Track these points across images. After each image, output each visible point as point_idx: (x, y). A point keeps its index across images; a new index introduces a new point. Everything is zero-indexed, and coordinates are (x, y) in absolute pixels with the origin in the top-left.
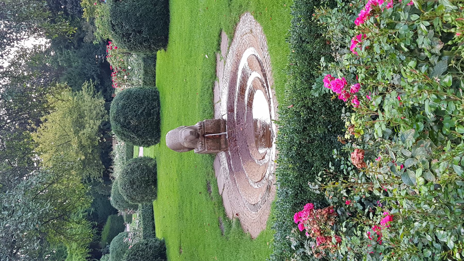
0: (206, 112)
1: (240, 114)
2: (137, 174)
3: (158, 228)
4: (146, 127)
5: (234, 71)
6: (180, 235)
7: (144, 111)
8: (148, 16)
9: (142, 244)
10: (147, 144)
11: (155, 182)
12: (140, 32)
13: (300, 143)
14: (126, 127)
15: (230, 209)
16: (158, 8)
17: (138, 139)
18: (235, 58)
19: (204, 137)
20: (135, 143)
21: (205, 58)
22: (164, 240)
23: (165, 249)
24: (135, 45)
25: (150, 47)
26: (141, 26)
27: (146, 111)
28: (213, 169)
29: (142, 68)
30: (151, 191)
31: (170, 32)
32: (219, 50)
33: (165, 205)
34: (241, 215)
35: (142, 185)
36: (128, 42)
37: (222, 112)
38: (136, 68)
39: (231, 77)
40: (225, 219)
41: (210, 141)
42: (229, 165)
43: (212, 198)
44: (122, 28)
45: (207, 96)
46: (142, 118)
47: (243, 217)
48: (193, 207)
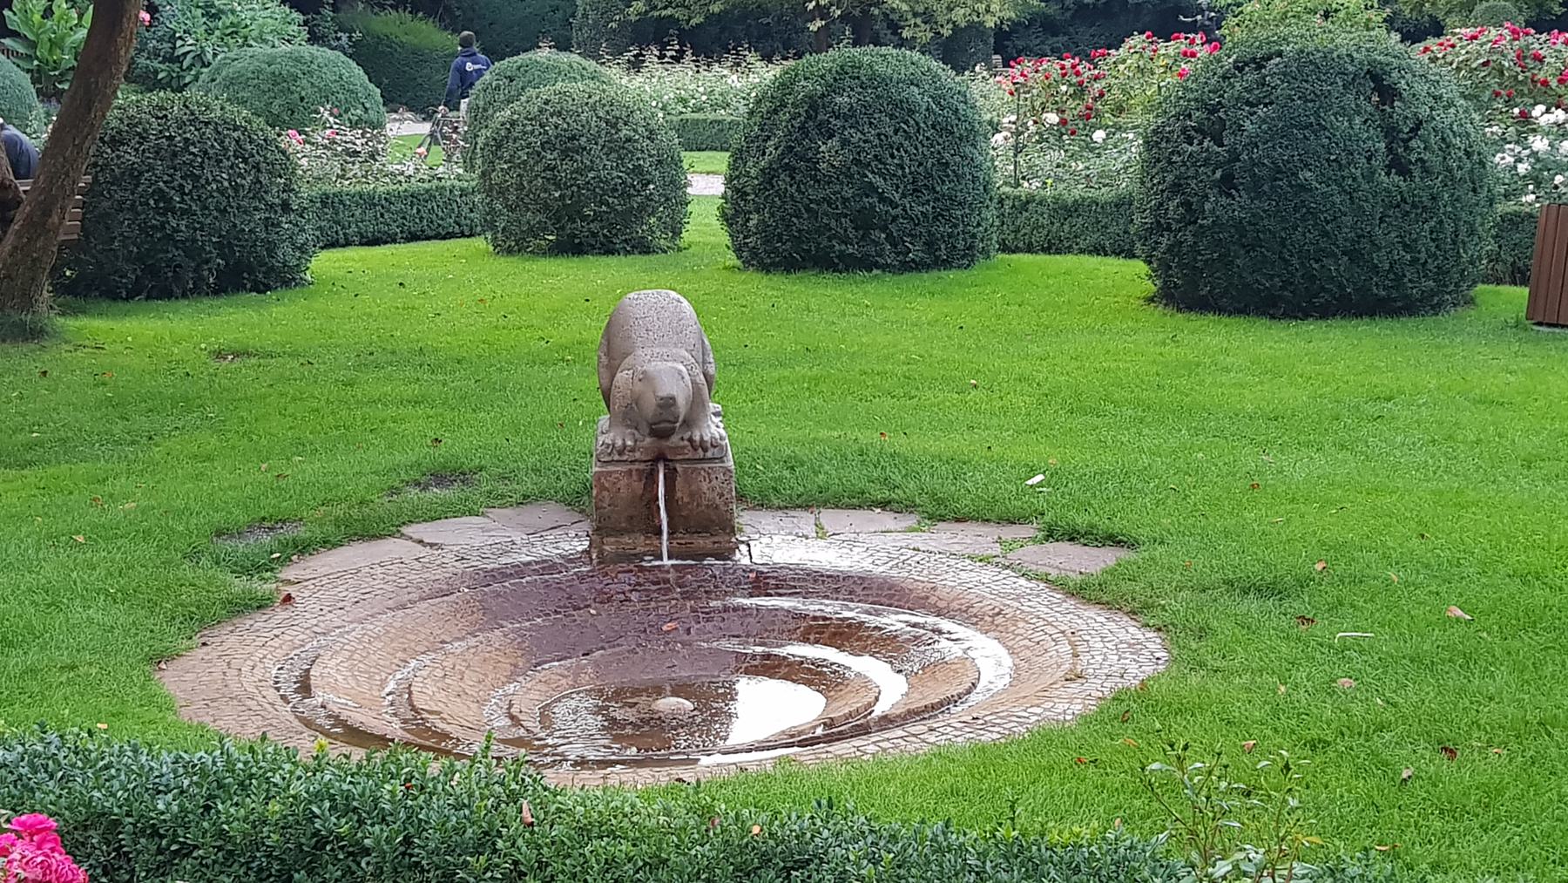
0: (786, 473)
1: (734, 621)
2: (608, 168)
3: (362, 259)
4: (808, 210)
5: (933, 600)
6: (294, 355)
7: (882, 199)
8: (1303, 219)
9: (287, 189)
10: (733, 215)
11: (571, 247)
12: (1227, 184)
13: (366, 852)
14: (809, 117)
15: (324, 570)
16: (1338, 267)
17: (753, 172)
18: (991, 603)
19: (655, 461)
20: (738, 158)
21: (1032, 471)
22: (302, 283)
23: (261, 288)
24: (1170, 163)
25: (1160, 227)
26: (1256, 190)
27: (880, 207)
28: (526, 499)
29: (1092, 194)
30: (531, 229)
31: (1225, 319)
32: (1051, 535)
33: (460, 286)
34: (281, 614)
35: (558, 186)
36: (1184, 130)
37: (771, 542)
38: (1096, 165)
39: (908, 584)
40: (284, 546)
41: (638, 487)
42: (520, 570)
43: (394, 491)
44: (1248, 103)
45: (856, 477)
46: (848, 192)
47: (274, 621)
48: (391, 411)
